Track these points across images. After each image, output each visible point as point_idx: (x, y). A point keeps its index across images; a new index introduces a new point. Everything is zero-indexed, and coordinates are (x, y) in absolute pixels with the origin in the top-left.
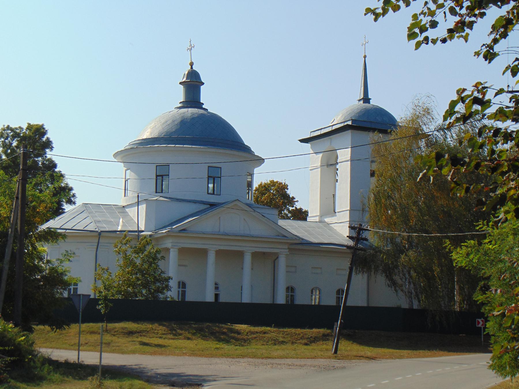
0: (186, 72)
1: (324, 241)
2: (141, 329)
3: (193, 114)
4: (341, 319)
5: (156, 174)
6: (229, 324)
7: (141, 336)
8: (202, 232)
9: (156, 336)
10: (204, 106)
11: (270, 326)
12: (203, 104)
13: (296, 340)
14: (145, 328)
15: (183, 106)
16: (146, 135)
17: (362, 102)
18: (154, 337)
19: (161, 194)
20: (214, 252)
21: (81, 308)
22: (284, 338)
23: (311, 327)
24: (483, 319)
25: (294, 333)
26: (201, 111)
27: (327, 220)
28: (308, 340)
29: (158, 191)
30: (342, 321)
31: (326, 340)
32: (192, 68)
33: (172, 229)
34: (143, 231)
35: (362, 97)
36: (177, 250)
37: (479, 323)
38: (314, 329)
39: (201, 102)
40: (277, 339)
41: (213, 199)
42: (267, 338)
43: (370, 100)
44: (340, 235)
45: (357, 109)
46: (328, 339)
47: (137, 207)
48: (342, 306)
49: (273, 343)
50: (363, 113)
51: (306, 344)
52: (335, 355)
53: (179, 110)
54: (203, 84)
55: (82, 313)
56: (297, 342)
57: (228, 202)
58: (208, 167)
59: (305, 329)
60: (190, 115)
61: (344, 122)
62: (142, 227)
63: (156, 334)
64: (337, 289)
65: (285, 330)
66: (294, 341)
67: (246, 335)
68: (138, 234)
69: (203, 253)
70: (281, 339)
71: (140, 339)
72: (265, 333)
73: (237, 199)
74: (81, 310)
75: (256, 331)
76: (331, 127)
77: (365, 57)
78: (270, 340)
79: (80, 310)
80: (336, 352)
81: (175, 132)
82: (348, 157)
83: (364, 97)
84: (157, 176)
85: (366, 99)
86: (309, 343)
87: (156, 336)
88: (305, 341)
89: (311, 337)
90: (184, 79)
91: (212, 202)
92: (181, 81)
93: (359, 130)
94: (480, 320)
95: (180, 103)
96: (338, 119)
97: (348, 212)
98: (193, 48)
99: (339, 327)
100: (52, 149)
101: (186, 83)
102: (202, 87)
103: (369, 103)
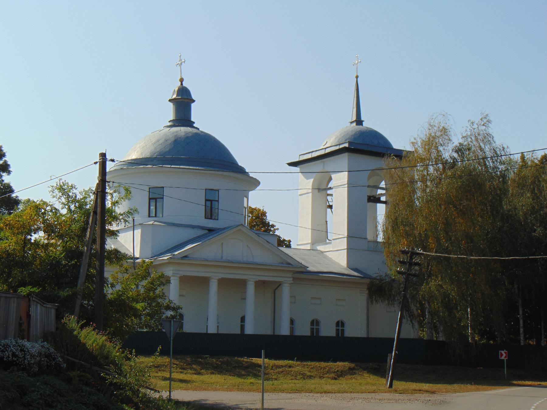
0: (177, 89)
1: (314, 269)
2: (158, 364)
3: (187, 133)
4: (396, 350)
5: (149, 197)
6: (246, 358)
7: (160, 371)
8: (204, 259)
9: (176, 371)
10: (195, 125)
11: (292, 359)
12: (194, 123)
13: (323, 375)
14: (163, 362)
15: (174, 125)
16: (134, 156)
17: (354, 124)
18: (174, 372)
19: (155, 219)
20: (216, 281)
21: (172, 335)
22: (310, 372)
23: (335, 361)
24: (506, 351)
25: (319, 367)
26: (195, 131)
27: (320, 248)
28: (335, 374)
29: (151, 215)
30: (397, 352)
31: (353, 374)
32: (182, 84)
33: (174, 255)
34: (138, 258)
35: (354, 118)
36: (178, 278)
37: (502, 355)
38: (338, 363)
39: (192, 120)
40: (304, 373)
41: (211, 224)
42: (294, 372)
43: (363, 122)
44: (339, 265)
45: (352, 130)
46: (354, 372)
47: (132, 232)
48: (396, 338)
49: (302, 377)
50: (359, 135)
51: (335, 379)
52: (390, 389)
53: (170, 128)
54: (194, 101)
55: (173, 340)
56: (324, 376)
57: (231, 227)
58: (218, 219)
59: (328, 363)
60: (183, 134)
61: (339, 145)
62: (137, 255)
63: (175, 369)
64: (311, 320)
65: (309, 363)
66: (322, 375)
67: (272, 369)
68: (134, 261)
69: (205, 281)
70: (308, 374)
71: (159, 374)
72: (290, 367)
73: (241, 224)
74: (172, 337)
75: (281, 364)
76: (324, 150)
77: (357, 77)
78: (298, 374)
79: (170, 337)
80: (391, 386)
81: (169, 152)
82: (345, 181)
83: (356, 119)
84: (150, 199)
85: (359, 122)
86: (336, 377)
87: (176, 371)
88: (333, 375)
89: (338, 371)
90: (174, 96)
91: (210, 228)
92: (170, 98)
93: (355, 153)
94: (503, 352)
95: (169, 122)
96: (331, 141)
97: (346, 239)
98: (183, 63)
99: (394, 359)
100: (10, 173)
101: (177, 100)
102: (193, 105)
103: (362, 125)
